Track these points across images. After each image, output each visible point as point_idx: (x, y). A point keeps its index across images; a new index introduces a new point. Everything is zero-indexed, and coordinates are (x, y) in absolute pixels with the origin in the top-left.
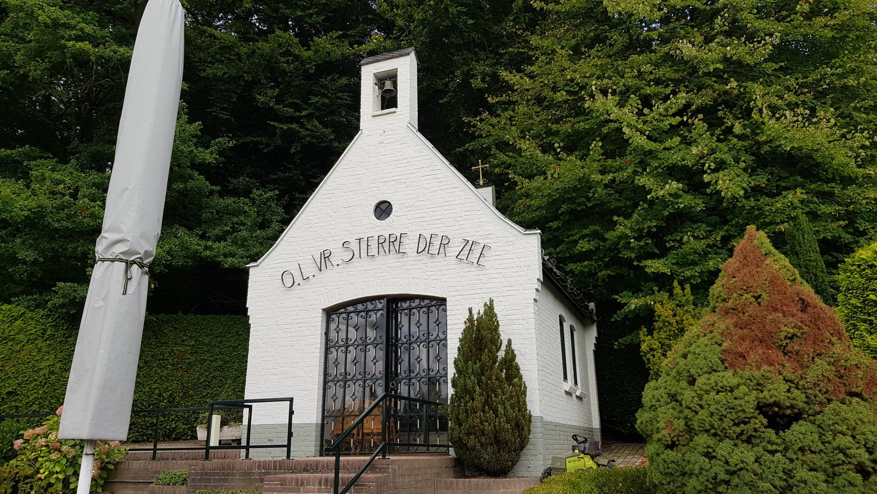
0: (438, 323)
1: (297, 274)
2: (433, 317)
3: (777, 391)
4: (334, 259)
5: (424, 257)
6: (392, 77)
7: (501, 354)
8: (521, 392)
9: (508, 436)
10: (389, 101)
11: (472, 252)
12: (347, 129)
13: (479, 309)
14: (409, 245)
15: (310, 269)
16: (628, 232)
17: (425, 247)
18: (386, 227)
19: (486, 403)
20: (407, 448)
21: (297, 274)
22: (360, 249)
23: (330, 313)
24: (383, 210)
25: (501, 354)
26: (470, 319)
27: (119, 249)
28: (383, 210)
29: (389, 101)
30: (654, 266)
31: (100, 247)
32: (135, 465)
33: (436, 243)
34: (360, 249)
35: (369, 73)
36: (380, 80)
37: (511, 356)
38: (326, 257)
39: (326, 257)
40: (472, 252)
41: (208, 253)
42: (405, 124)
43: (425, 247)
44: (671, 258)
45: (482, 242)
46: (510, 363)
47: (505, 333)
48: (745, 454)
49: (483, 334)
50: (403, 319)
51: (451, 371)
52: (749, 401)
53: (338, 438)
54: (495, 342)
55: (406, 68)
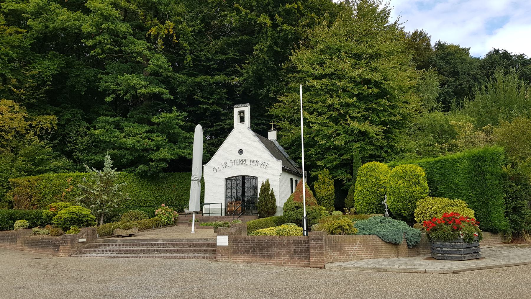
0: (255, 183)
1: (217, 168)
2: (254, 181)
3: (297, 205)
4: (228, 165)
5: (252, 166)
6: (243, 112)
7: (270, 192)
8: (274, 201)
9: (271, 211)
10: (242, 120)
11: (264, 165)
12: (231, 128)
13: (265, 181)
14: (248, 162)
15: (221, 168)
16: (313, 153)
17: (252, 163)
18: (242, 157)
19: (266, 203)
20: (248, 214)
21: (217, 168)
22: (234, 163)
23: (226, 179)
24: (241, 152)
25: (270, 192)
26: (263, 184)
27: (196, 179)
28: (241, 152)
29: (242, 120)
30: (319, 163)
31: (192, 178)
32: (181, 218)
33: (255, 162)
34: (234, 163)
35: (236, 110)
36: (240, 112)
37: (272, 192)
38: (225, 164)
39: (225, 164)
40: (264, 165)
41: (183, 155)
42: (247, 127)
43: (252, 163)
44: (325, 160)
45: (267, 163)
46: (272, 195)
47: (271, 187)
48: (292, 213)
49: (266, 187)
50: (246, 181)
51: (258, 196)
52: (293, 206)
53: (229, 212)
54: (269, 189)
55: (247, 109)
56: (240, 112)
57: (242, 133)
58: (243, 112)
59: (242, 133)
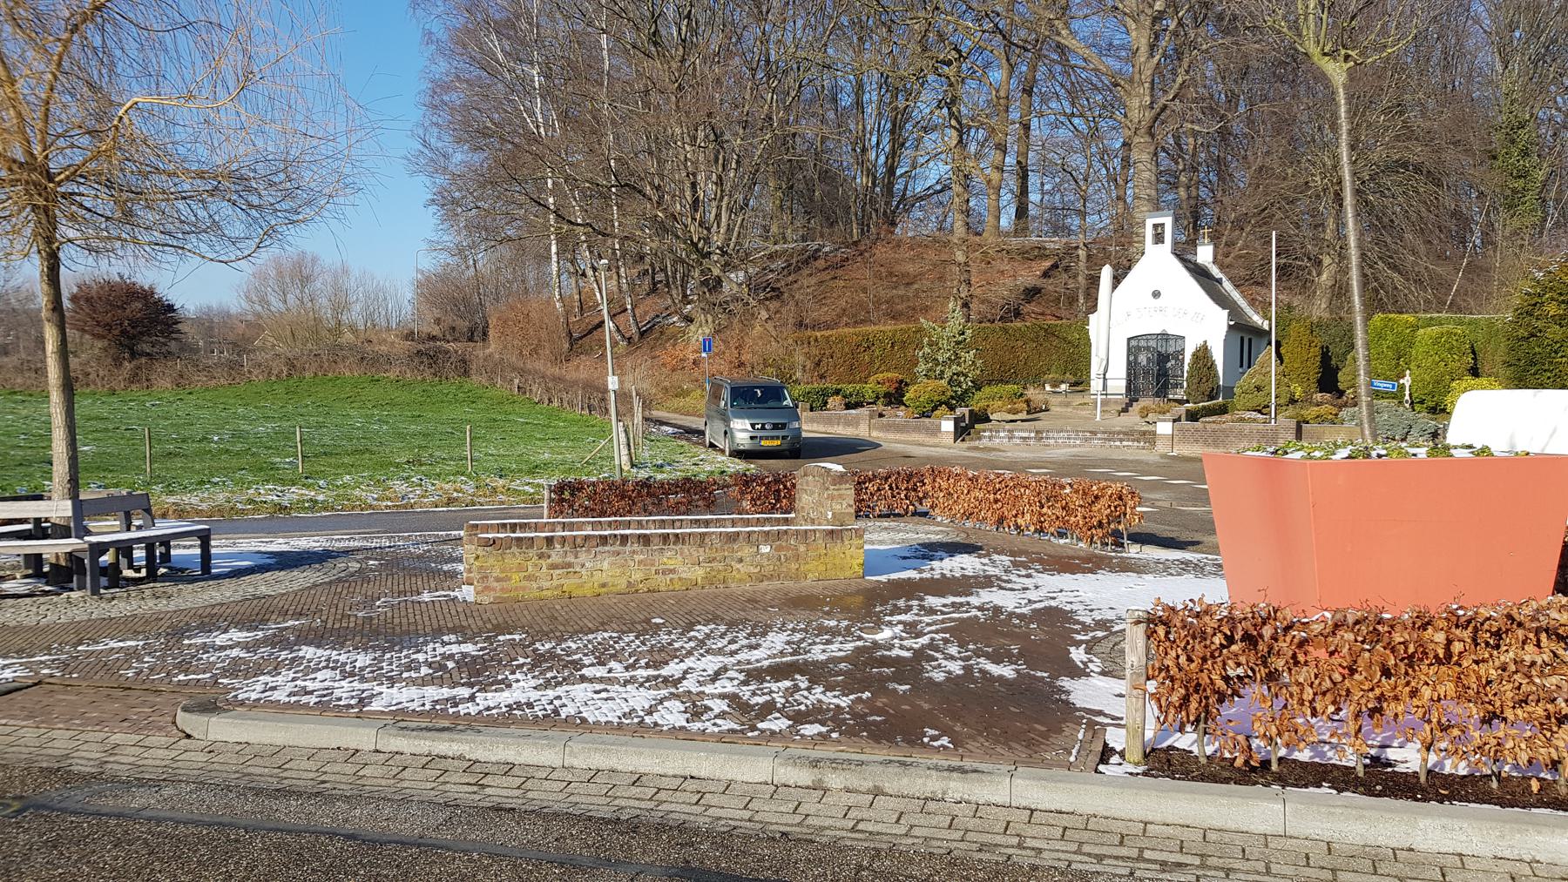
6: (1162, 225)
10: (1159, 238)
24: (1156, 294)
28: (1156, 294)
29: (1159, 238)
35: (1150, 223)
36: (1155, 226)
49: (1203, 354)
51: (1186, 368)
56: (1155, 226)
57: (1157, 264)
58: (1162, 225)
59: (1157, 264)
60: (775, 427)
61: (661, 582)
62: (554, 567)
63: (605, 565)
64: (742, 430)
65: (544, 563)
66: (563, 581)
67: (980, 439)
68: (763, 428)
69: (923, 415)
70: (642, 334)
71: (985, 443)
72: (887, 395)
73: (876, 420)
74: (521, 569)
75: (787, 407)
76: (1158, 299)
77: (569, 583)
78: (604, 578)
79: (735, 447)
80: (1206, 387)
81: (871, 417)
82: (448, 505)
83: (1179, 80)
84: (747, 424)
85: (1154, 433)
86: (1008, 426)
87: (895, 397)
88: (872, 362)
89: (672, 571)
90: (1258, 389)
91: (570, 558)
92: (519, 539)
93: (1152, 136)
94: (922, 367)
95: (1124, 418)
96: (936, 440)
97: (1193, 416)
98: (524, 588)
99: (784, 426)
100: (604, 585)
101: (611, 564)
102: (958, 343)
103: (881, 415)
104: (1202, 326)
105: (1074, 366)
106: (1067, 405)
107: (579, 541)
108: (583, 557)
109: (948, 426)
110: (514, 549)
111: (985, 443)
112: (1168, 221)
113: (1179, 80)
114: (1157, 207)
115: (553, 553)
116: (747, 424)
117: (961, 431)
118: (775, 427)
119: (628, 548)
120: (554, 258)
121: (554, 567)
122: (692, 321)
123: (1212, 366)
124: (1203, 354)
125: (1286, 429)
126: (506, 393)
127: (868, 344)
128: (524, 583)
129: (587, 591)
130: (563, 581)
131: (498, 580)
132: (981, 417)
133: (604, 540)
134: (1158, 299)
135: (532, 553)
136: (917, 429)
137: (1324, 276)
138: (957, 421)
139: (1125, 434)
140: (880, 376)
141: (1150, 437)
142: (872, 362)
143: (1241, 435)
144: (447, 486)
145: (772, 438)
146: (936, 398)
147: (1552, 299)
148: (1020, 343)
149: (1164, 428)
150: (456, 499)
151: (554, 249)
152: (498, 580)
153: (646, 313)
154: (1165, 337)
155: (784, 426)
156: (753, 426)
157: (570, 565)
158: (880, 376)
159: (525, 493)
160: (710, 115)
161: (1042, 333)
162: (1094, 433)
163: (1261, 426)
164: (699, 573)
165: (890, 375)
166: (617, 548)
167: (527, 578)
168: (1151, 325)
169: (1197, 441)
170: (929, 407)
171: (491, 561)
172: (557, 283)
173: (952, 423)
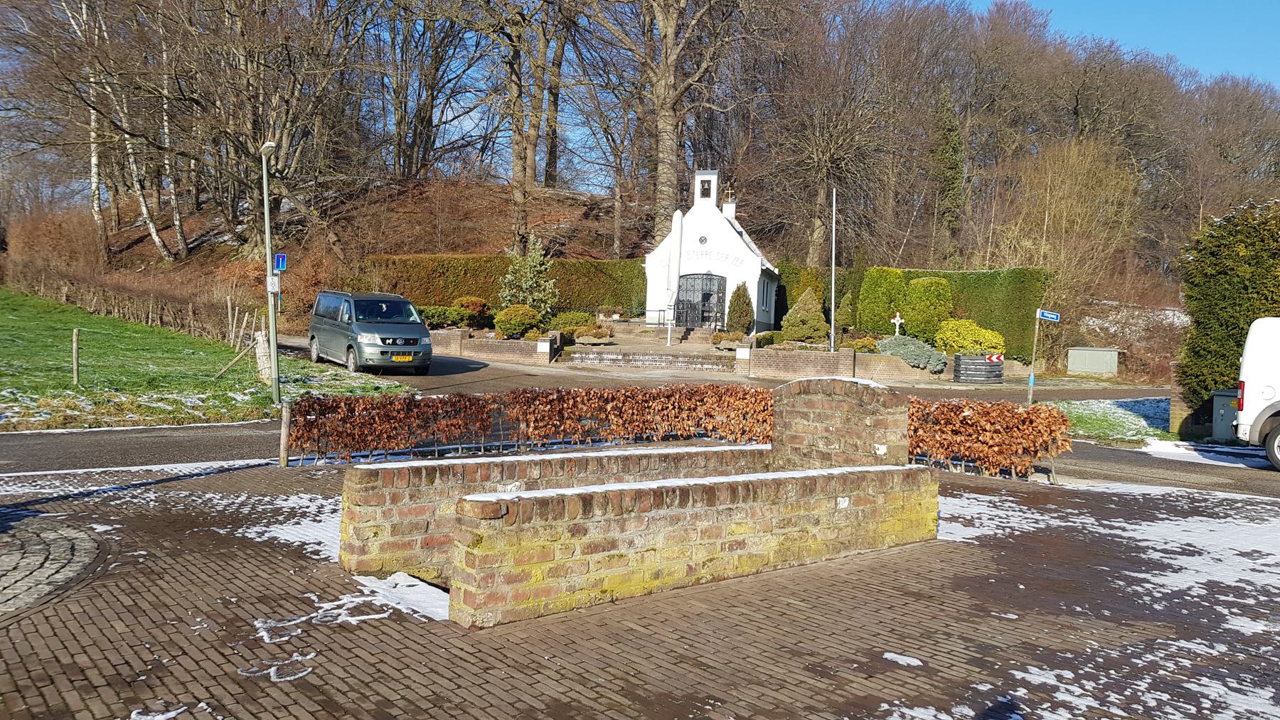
6: (709, 182)
24: (703, 240)
28: (703, 240)
35: (699, 178)
49: (741, 292)
58: (709, 182)
60: (407, 342)
61: (730, 563)
62: (592, 548)
63: (660, 541)
64: (371, 345)
65: (579, 543)
66: (603, 573)
67: (572, 359)
68: (394, 343)
69: (510, 337)
70: (190, 251)
71: (577, 363)
72: (471, 318)
73: (467, 340)
74: (545, 555)
75: (414, 323)
76: (706, 244)
77: (611, 576)
78: (653, 562)
79: (363, 362)
80: (745, 320)
81: (463, 338)
82: (64, 425)
83: (704, 65)
84: (377, 339)
85: (734, 358)
86: (595, 349)
87: (482, 321)
88: (446, 287)
89: (741, 544)
90: (804, 322)
91: (615, 534)
92: (543, 503)
93: (674, 110)
94: (506, 293)
95: (685, 345)
96: (531, 361)
97: (760, 344)
98: (548, 592)
99: (415, 342)
100: (657, 575)
101: (667, 538)
102: (540, 272)
103: (471, 337)
104: (743, 267)
105: (631, 302)
106: (630, 332)
107: (627, 502)
108: (632, 527)
109: (544, 347)
110: (537, 522)
111: (577, 363)
112: (713, 178)
113: (704, 65)
114: (702, 166)
115: (590, 525)
116: (377, 339)
117: (555, 353)
118: (407, 342)
119: (689, 510)
120: (94, 170)
121: (592, 548)
122: (246, 241)
123: (749, 304)
124: (741, 292)
125: (846, 357)
126: (52, 302)
127: (442, 270)
128: (551, 582)
129: (635, 588)
130: (603, 573)
131: (510, 580)
132: (568, 340)
133: (659, 496)
134: (706, 244)
135: (562, 525)
136: (511, 350)
137: (815, 236)
138: (552, 342)
139: (703, 358)
140: (465, 299)
141: (730, 363)
142: (446, 287)
143: (807, 361)
144: (55, 402)
145: (404, 354)
146: (527, 321)
147: (1242, 241)
148: (574, 277)
149: (743, 353)
150: (74, 418)
151: (94, 160)
152: (510, 580)
153: (192, 231)
154: (709, 277)
155: (415, 342)
156: (383, 340)
157: (613, 545)
158: (465, 299)
159: (163, 411)
160: (287, 39)
161: (593, 269)
162: (676, 356)
163: (824, 354)
164: (767, 545)
165: (473, 299)
166: (675, 511)
167: (554, 573)
168: (697, 265)
169: (770, 365)
170: (519, 330)
171: (501, 545)
172: (91, 194)
173: (548, 345)
